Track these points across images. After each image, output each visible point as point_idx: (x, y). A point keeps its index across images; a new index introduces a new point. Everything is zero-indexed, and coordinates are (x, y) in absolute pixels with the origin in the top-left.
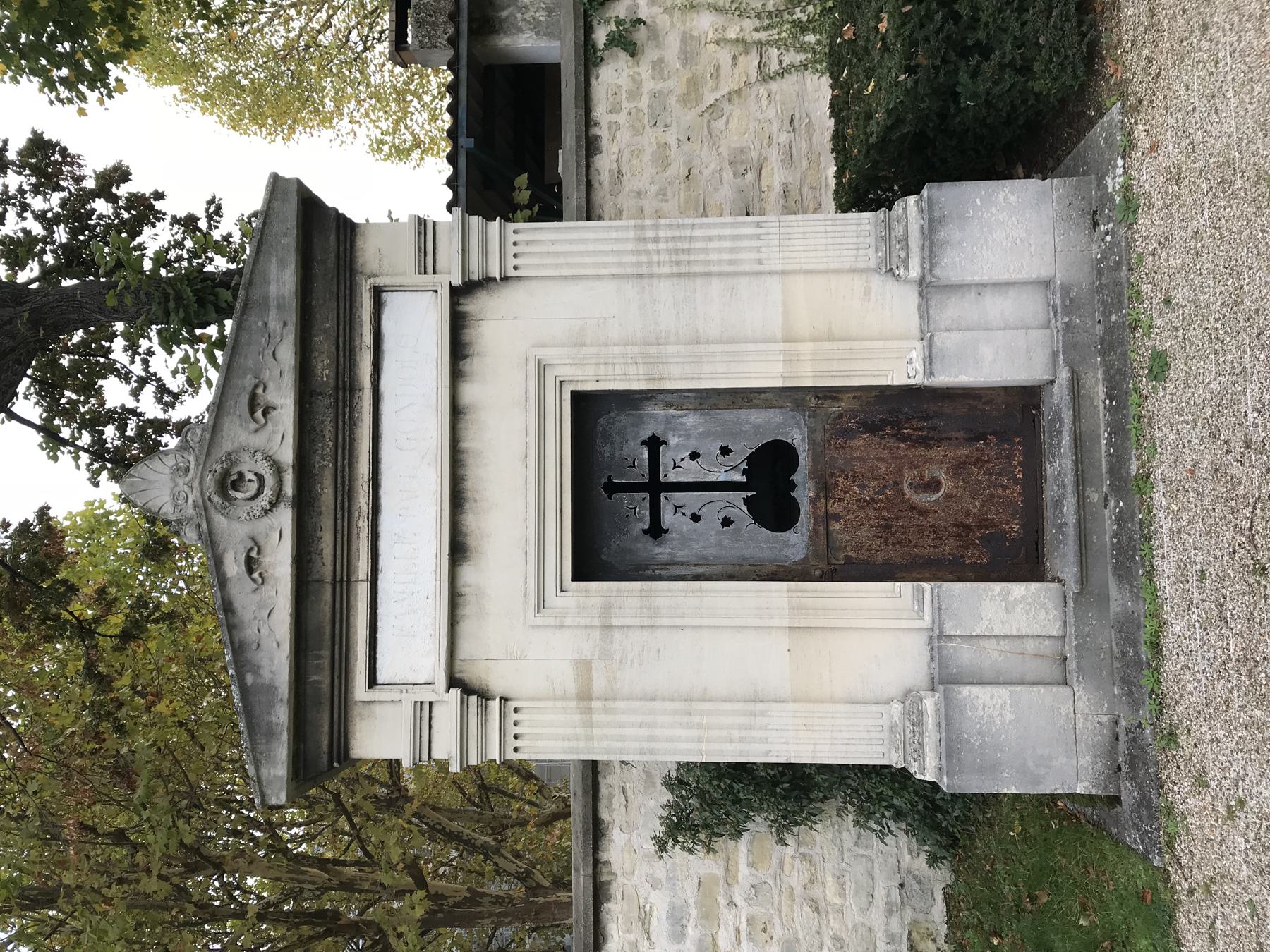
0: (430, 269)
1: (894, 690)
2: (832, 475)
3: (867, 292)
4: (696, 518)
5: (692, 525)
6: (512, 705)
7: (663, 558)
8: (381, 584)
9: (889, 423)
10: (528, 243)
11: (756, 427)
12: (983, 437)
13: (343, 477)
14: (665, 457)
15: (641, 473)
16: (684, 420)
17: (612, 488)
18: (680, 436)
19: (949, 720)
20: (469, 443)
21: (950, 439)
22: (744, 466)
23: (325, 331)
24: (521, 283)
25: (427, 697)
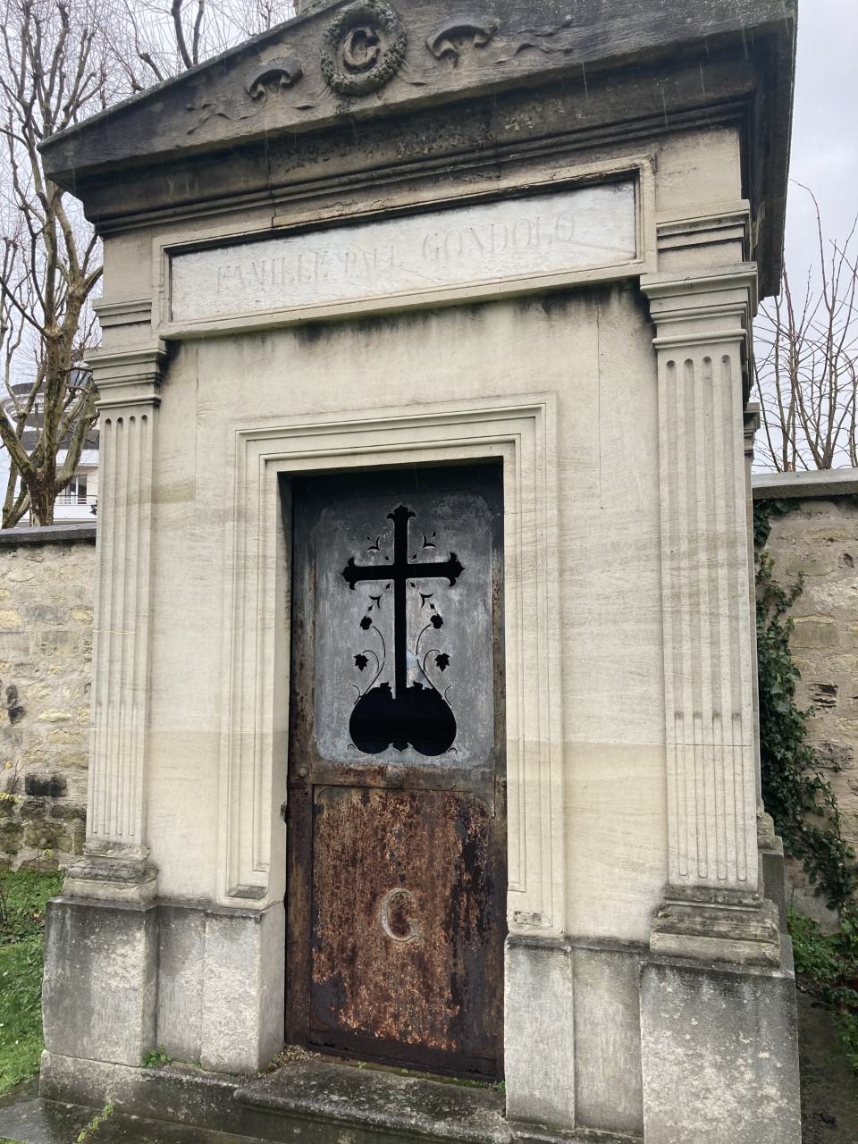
0: (665, 244)
1: (158, 856)
2: (413, 797)
3: (635, 867)
4: (366, 623)
5: (353, 619)
6: (150, 413)
7: (323, 584)
8: (272, 246)
9: (474, 881)
10: (708, 379)
11: (470, 703)
12: (456, 999)
13: (388, 176)
14: (435, 584)
15: (420, 554)
16: (481, 608)
17: (401, 518)
18: (461, 603)
19: (113, 912)
20: (437, 330)
21: (455, 956)
22: (425, 685)
23: (571, 113)
24: (651, 376)
25: (155, 317)
